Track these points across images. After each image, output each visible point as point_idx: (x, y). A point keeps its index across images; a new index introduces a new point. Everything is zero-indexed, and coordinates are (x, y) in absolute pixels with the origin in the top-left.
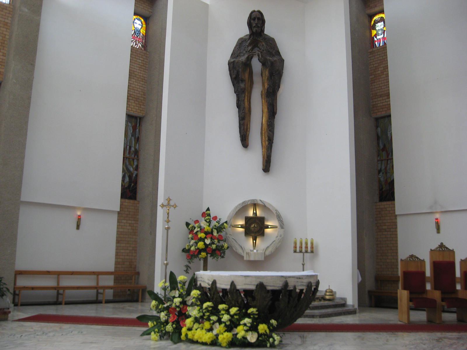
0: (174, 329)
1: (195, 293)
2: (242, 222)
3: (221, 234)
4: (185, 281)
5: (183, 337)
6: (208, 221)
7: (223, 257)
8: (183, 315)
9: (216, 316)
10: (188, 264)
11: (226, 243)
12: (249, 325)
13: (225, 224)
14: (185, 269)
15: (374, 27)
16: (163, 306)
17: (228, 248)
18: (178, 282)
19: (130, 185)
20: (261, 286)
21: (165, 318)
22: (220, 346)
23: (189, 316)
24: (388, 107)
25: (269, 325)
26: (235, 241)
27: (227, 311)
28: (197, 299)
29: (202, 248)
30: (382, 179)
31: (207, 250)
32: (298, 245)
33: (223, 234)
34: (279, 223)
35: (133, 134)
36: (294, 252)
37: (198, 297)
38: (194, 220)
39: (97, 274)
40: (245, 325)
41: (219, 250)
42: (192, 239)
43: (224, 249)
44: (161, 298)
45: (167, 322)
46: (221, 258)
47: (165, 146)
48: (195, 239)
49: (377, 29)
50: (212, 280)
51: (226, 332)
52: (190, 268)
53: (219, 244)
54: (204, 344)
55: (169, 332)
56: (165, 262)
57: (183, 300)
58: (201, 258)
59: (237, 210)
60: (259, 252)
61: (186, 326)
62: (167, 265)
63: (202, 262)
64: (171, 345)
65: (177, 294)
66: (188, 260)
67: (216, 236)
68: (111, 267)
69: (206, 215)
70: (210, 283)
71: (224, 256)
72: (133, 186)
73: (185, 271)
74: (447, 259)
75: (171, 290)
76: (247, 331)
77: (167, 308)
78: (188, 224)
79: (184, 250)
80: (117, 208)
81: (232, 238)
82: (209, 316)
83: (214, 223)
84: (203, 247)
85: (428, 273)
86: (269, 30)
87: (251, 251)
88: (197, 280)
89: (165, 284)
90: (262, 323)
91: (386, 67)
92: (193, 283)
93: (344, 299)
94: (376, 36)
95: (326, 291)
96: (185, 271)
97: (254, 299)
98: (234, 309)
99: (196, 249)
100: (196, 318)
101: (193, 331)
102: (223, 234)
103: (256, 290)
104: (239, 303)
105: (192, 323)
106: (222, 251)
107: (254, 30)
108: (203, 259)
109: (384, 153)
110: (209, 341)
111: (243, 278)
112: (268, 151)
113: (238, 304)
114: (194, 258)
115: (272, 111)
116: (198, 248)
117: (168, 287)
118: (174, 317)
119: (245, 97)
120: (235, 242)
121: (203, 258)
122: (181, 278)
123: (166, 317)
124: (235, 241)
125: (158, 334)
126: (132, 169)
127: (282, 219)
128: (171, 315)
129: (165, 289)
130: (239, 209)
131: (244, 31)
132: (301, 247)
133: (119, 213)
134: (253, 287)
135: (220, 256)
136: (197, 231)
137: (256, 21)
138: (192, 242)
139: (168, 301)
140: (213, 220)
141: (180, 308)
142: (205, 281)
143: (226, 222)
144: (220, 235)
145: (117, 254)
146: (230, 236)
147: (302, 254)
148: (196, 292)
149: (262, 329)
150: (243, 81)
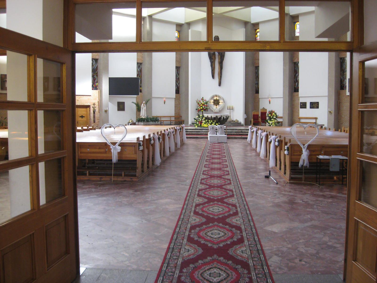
1: (204, 118)
2: (213, 101)
5: (202, 126)
8: (201, 123)
15: (256, 34)
19: (177, 89)
20: (217, 117)
27: (210, 121)
32: (232, 108)
35: (177, 73)
39: (170, 117)
49: (257, 35)
65: (200, 119)
68: (173, 115)
74: (265, 111)
83: (205, 102)
85: (260, 115)
92: (203, 116)
93: (241, 122)
94: (257, 37)
97: (215, 119)
111: (214, 116)
115: (221, 68)
126: (177, 84)
129: (197, 118)
132: (229, 108)
134: (215, 117)
138: (199, 107)
150: (212, 59)
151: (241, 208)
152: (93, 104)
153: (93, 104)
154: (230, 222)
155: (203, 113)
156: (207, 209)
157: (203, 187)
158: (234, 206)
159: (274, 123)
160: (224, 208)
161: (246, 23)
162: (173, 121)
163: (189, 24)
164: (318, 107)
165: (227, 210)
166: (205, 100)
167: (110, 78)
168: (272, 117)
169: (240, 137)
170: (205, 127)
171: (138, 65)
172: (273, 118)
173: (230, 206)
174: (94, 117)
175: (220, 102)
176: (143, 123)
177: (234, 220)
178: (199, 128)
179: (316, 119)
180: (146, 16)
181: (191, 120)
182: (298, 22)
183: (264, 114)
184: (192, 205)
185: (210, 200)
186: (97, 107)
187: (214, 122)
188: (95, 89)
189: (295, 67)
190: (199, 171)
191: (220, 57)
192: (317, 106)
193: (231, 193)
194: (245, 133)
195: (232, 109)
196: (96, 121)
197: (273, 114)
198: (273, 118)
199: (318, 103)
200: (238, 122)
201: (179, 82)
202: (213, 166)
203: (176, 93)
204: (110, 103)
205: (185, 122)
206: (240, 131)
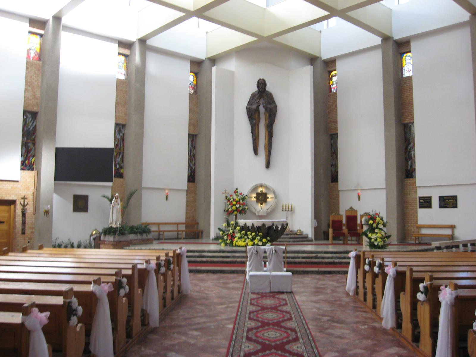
1: (238, 228)
2: (255, 195)
5: (234, 244)
6: (237, 195)
8: (232, 237)
12: (259, 239)
13: (246, 197)
15: (331, 79)
17: (248, 209)
20: (264, 225)
23: (236, 237)
24: (336, 129)
25: (267, 239)
27: (251, 234)
28: (239, 230)
30: (333, 170)
32: (287, 207)
33: (245, 202)
35: (192, 145)
39: (177, 224)
40: (258, 239)
48: (231, 205)
49: (333, 80)
59: (252, 189)
65: (230, 229)
70: (244, 224)
72: (193, 175)
74: (353, 214)
75: (228, 227)
76: (258, 241)
77: (227, 235)
80: (186, 188)
83: (240, 196)
85: (344, 221)
86: (269, 88)
90: (264, 238)
91: (336, 106)
92: (237, 224)
93: (307, 235)
94: (332, 84)
95: (298, 230)
97: (261, 230)
105: (237, 239)
107: (261, 90)
109: (334, 155)
111: (257, 222)
112: (268, 158)
119: (256, 128)
126: (192, 165)
129: (225, 227)
131: (255, 89)
133: (187, 191)
136: (232, 201)
137: (261, 84)
143: (247, 196)
145: (186, 213)
147: (286, 212)
150: (254, 119)
151: (301, 333)
152: (22, 198)
153: (22, 198)
154: (290, 349)
155: (236, 218)
156: (261, 335)
157: (254, 308)
158: (294, 330)
159: (380, 238)
160: (282, 333)
161: (313, 60)
162: (182, 231)
163: (213, 60)
164: (455, 206)
165: (285, 335)
166: (241, 194)
167: (57, 149)
168: (375, 225)
169: (316, 269)
170: (240, 246)
171: (118, 128)
172: (377, 227)
173: (289, 331)
174: (24, 223)
175: (268, 198)
176: (112, 237)
177: (295, 347)
178: (229, 248)
179: (453, 227)
180: (134, 40)
181: (213, 233)
182: (410, 52)
183: (352, 218)
184: (244, 330)
185: (265, 324)
186: (31, 203)
187: (258, 236)
188: (29, 170)
189: (405, 133)
190: (245, 300)
191: (268, 115)
192: (455, 202)
193: (288, 316)
194: (323, 260)
195: (290, 210)
196: (28, 231)
197: (378, 219)
198: (377, 227)
199: (455, 197)
200: (301, 233)
201: (194, 162)
202: (264, 302)
203: (189, 181)
204: (55, 196)
205: (204, 234)
206: (314, 255)
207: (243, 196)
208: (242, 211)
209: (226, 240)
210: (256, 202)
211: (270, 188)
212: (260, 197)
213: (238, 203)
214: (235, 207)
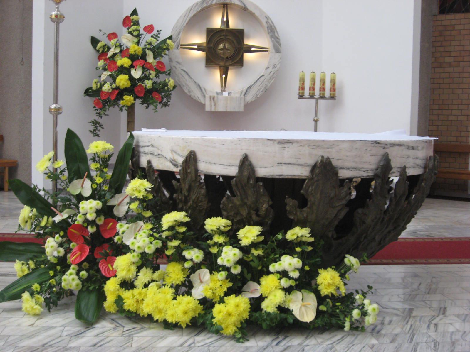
0: (84, 281)
2: (200, 39)
3: (162, 60)
4: (107, 156)
5: (109, 304)
6: (135, 33)
7: (166, 105)
8: (102, 245)
9: (199, 247)
10: (97, 118)
11: (172, 79)
12: (295, 275)
13: (169, 41)
14: (92, 128)
16: (51, 220)
17: (174, 87)
18: (89, 157)
21: (59, 252)
22: (218, 331)
23: (122, 249)
26: (188, 74)
27: (233, 239)
29: (125, 86)
31: (136, 90)
32: (307, 85)
33: (165, 60)
34: (272, 41)
36: (299, 98)
37: (146, 197)
38: (108, 33)
40: (284, 274)
41: (159, 91)
42: (105, 69)
43: (168, 88)
44: (46, 198)
45: (63, 264)
46: (162, 107)
47: (42, 48)
50: (186, 153)
51: (233, 296)
52: (101, 126)
53: (158, 80)
54: (169, 326)
55: (71, 293)
56: (53, 106)
57: (104, 203)
58: (123, 106)
59: (191, 15)
60: (232, 95)
61: (115, 276)
62: (57, 112)
63: (125, 114)
64: (78, 335)
65: (87, 188)
66: (97, 110)
67: (152, 63)
69: (132, 24)
70: (180, 160)
71: (169, 103)
73: (91, 131)
76: (288, 290)
77: (64, 226)
78: (94, 41)
79: (88, 92)
81: (182, 70)
82: (179, 250)
83: (147, 38)
84: (128, 84)
87: (218, 94)
88: (139, 152)
89: (53, 162)
96: (91, 131)
97: (303, 202)
98: (249, 231)
99: (113, 89)
100: (143, 255)
101: (135, 291)
102: (165, 60)
103: (311, 179)
104: (262, 213)
105: (134, 268)
106: (163, 94)
108: (127, 108)
110: (185, 319)
113: (258, 215)
114: (109, 107)
116: (116, 86)
117: (62, 171)
118: (81, 249)
120: (186, 77)
121: (127, 106)
122: (96, 147)
123: (62, 250)
124: (188, 74)
125: (42, 299)
127: (278, 35)
128: (73, 245)
130: (195, 13)
132: (313, 89)
135: (161, 102)
136: (115, 54)
138: (105, 75)
139: (65, 207)
140: (145, 33)
141: (98, 226)
142: (164, 154)
143: (170, 38)
144: (159, 62)
146: (178, 66)
147: (314, 101)
148: (141, 184)
149: (329, 285)
155: (131, 126)
195: (327, 93)
207: (156, 37)
208: (154, 93)
209: (53, 266)
210: (203, 63)
211: (257, 13)
212: (221, 46)
213: (139, 62)
214: (126, 77)
